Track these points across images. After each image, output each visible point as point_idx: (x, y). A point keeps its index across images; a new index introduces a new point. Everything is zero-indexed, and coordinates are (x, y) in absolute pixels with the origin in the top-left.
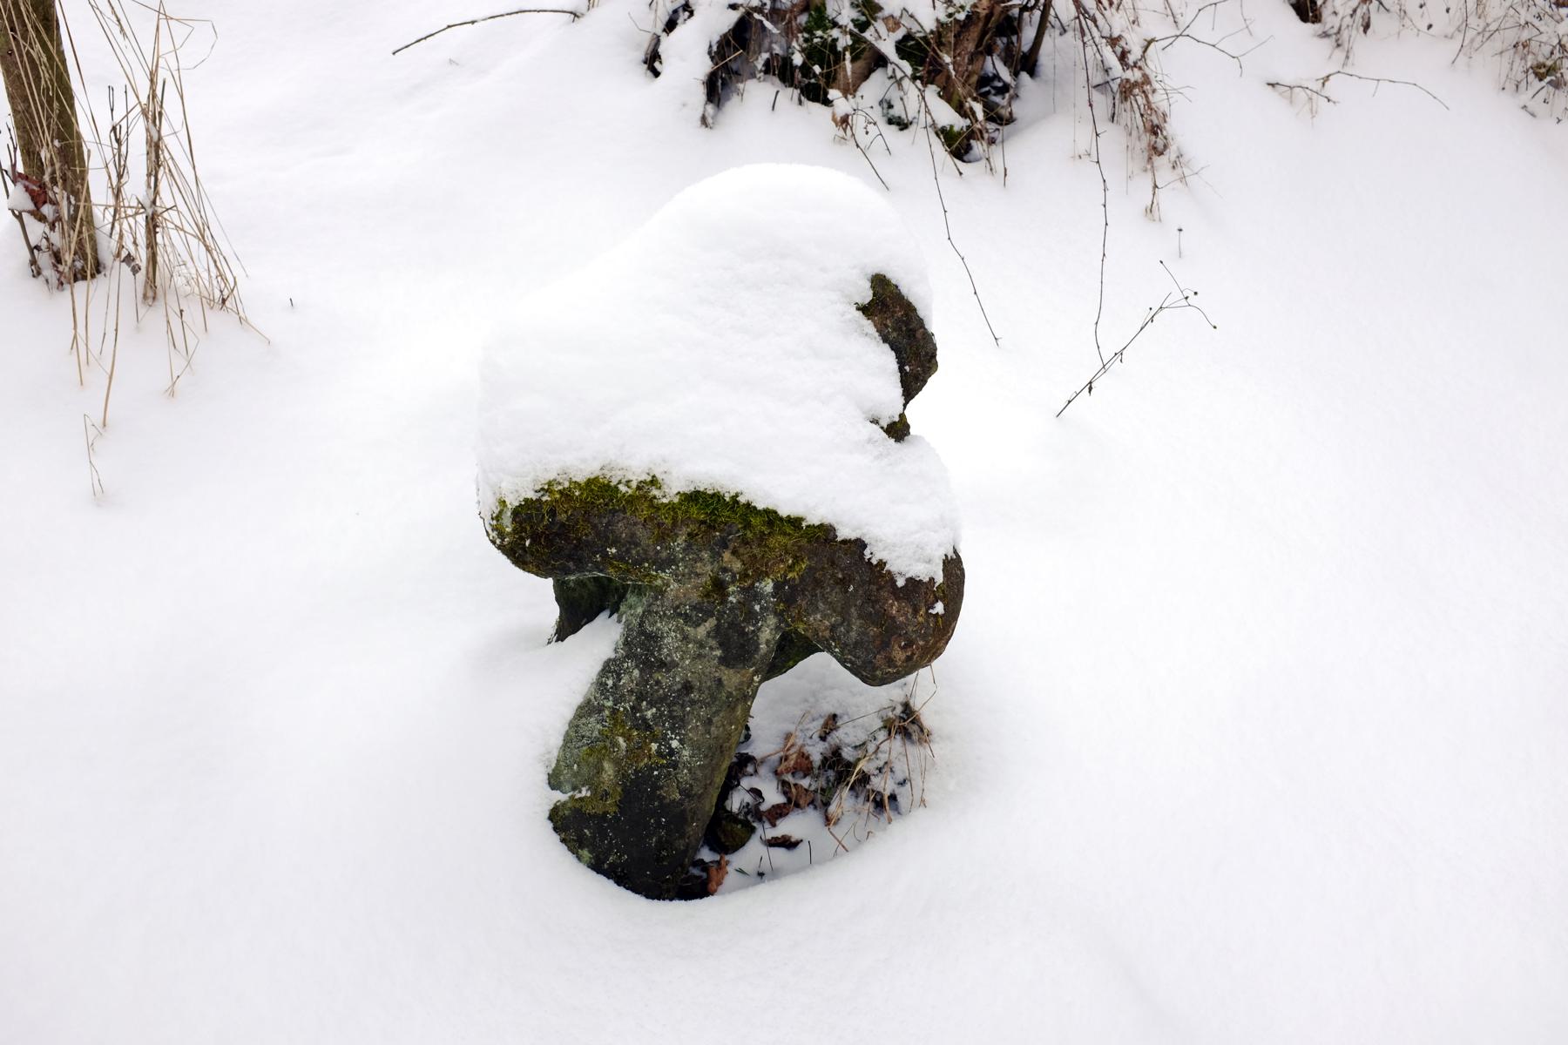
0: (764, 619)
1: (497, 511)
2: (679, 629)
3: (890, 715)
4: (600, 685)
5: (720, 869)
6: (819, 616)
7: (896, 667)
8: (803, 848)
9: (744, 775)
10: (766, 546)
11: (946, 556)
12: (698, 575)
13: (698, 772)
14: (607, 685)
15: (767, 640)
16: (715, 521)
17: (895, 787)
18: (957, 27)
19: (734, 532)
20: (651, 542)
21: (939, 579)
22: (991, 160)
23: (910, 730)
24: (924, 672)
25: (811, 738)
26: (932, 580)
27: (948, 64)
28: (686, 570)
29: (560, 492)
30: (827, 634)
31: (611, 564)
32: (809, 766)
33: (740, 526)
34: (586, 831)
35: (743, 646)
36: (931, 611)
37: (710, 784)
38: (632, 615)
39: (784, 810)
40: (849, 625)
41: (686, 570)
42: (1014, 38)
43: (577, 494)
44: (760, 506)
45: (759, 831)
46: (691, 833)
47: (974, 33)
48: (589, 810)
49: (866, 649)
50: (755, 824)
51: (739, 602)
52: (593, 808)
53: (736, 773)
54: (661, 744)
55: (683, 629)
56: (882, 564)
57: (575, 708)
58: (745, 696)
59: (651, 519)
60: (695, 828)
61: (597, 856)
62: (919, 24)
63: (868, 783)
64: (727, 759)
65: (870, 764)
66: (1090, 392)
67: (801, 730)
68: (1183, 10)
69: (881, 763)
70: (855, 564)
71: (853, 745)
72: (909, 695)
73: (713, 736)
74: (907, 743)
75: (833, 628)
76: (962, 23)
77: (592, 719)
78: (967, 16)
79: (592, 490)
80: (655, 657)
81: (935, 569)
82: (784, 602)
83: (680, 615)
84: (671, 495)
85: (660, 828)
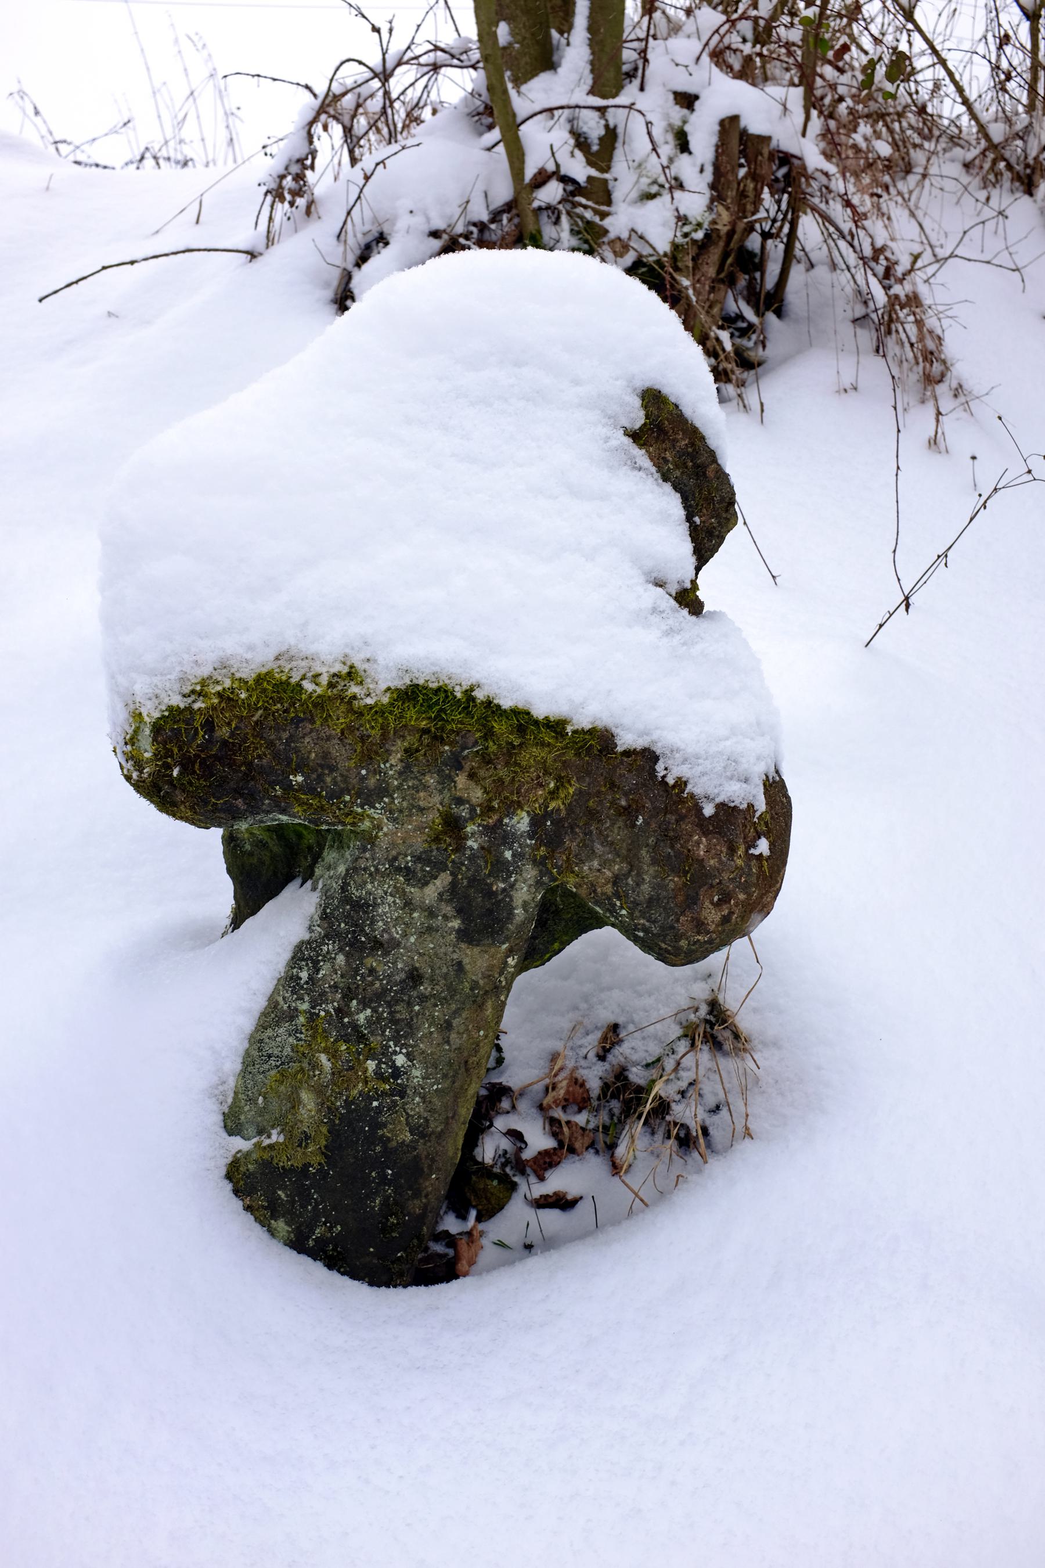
0: (519, 871)
1: (130, 731)
2: (399, 891)
3: (692, 1017)
4: (289, 981)
5: (472, 1242)
6: (595, 864)
7: (708, 932)
8: (583, 1209)
9: (498, 1113)
10: (516, 764)
11: (767, 777)
12: (422, 810)
13: (435, 1100)
14: (301, 979)
15: (525, 902)
16: (442, 729)
17: (705, 1116)
18: (695, 248)
19: (470, 745)
20: (352, 763)
21: (761, 806)
22: (744, 396)
23: (720, 1038)
24: (740, 944)
25: (586, 1057)
26: (751, 806)
27: (686, 288)
28: (405, 804)
29: (219, 695)
30: (609, 889)
31: (297, 799)
32: (585, 1096)
33: (478, 735)
34: (280, 1192)
35: (490, 912)
36: (752, 851)
37: (453, 1117)
38: (331, 878)
39: (555, 1158)
40: (639, 874)
41: (405, 804)
42: (758, 275)
43: (243, 696)
44: (506, 704)
45: (523, 1188)
46: (430, 1189)
47: (715, 254)
48: (283, 1162)
49: (665, 908)
50: (516, 1179)
51: (482, 848)
52: (289, 1160)
53: (487, 1111)
54: (380, 1062)
55: (403, 889)
56: (681, 783)
57: (257, 1015)
58: (496, 987)
59: (350, 728)
60: (436, 1183)
61: (298, 1228)
62: (651, 246)
63: (668, 1113)
64: (475, 1079)
65: (669, 1087)
66: (907, 610)
67: (572, 1048)
68: (943, 241)
69: (683, 1085)
70: (644, 785)
71: (644, 1063)
72: (716, 989)
73: (454, 1047)
74: (718, 1055)
75: (616, 880)
76: (700, 244)
77: (281, 1031)
78: (707, 236)
79: (264, 690)
80: (366, 935)
81: (754, 792)
82: (545, 845)
83: (399, 870)
84: (378, 692)
85: (385, 1184)
